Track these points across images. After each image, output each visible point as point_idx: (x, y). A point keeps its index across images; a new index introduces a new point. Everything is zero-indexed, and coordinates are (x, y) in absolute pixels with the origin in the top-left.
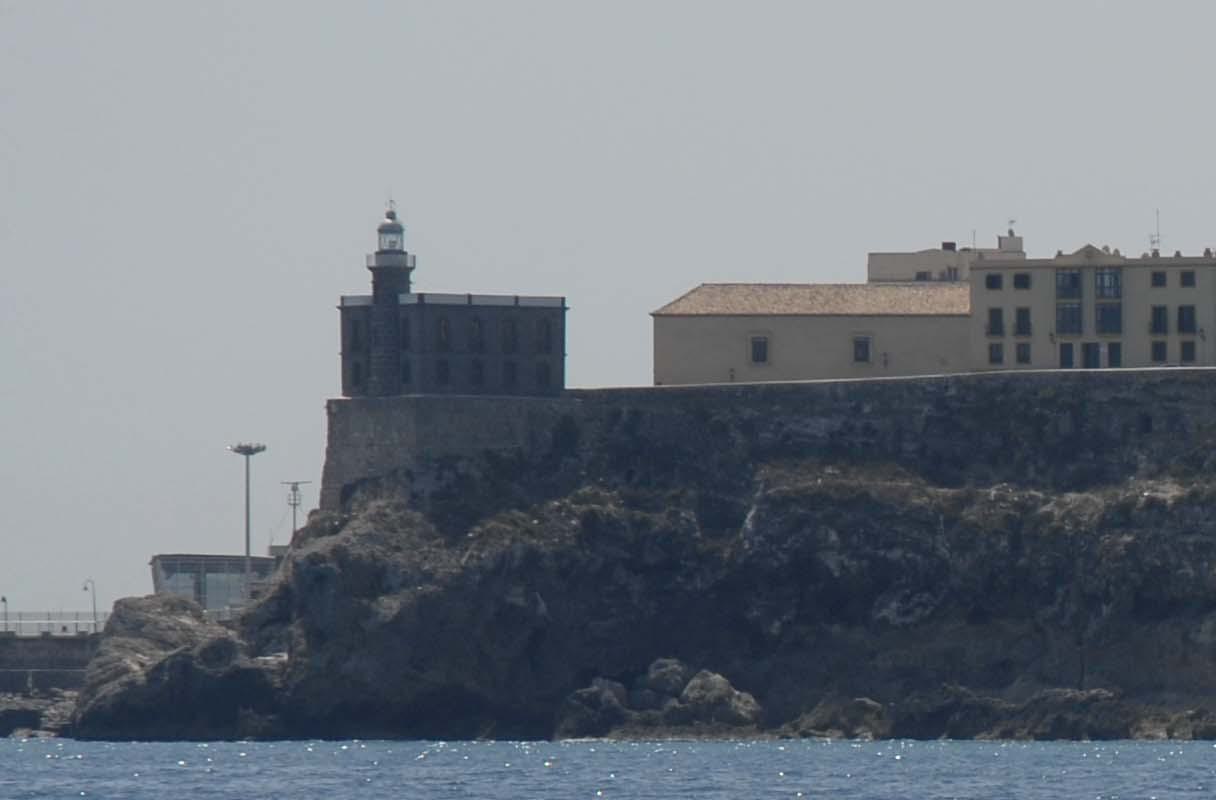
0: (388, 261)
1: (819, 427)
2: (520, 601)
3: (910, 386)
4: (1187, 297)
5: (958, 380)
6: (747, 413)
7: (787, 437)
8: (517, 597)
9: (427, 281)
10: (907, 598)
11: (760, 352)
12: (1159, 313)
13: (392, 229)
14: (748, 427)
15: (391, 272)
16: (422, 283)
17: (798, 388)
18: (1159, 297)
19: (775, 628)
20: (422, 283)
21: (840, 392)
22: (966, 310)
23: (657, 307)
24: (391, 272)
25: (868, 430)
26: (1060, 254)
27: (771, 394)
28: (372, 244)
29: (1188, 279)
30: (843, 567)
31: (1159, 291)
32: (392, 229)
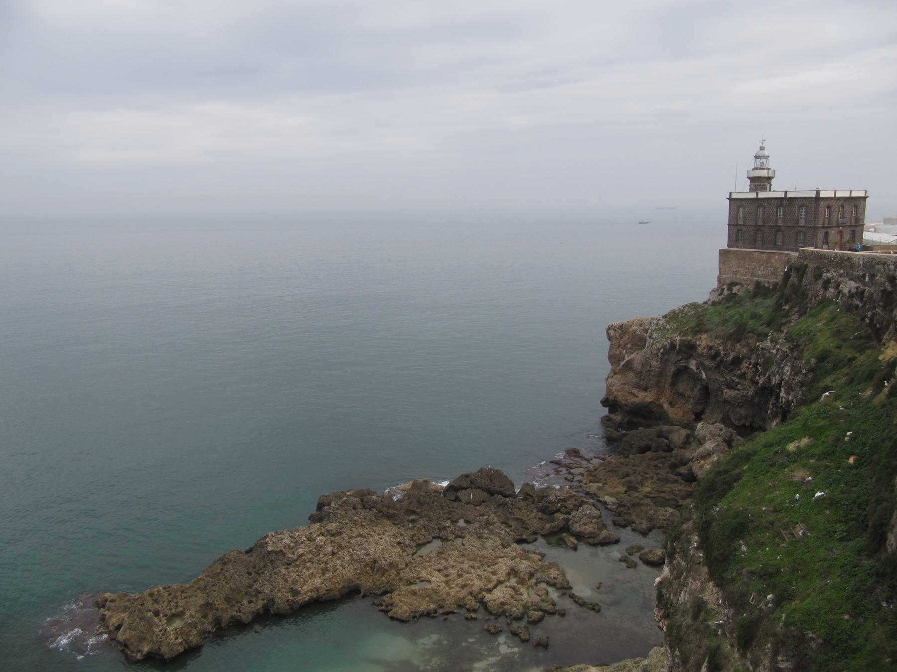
2: (694, 368)
15: (759, 183)
20: (778, 189)
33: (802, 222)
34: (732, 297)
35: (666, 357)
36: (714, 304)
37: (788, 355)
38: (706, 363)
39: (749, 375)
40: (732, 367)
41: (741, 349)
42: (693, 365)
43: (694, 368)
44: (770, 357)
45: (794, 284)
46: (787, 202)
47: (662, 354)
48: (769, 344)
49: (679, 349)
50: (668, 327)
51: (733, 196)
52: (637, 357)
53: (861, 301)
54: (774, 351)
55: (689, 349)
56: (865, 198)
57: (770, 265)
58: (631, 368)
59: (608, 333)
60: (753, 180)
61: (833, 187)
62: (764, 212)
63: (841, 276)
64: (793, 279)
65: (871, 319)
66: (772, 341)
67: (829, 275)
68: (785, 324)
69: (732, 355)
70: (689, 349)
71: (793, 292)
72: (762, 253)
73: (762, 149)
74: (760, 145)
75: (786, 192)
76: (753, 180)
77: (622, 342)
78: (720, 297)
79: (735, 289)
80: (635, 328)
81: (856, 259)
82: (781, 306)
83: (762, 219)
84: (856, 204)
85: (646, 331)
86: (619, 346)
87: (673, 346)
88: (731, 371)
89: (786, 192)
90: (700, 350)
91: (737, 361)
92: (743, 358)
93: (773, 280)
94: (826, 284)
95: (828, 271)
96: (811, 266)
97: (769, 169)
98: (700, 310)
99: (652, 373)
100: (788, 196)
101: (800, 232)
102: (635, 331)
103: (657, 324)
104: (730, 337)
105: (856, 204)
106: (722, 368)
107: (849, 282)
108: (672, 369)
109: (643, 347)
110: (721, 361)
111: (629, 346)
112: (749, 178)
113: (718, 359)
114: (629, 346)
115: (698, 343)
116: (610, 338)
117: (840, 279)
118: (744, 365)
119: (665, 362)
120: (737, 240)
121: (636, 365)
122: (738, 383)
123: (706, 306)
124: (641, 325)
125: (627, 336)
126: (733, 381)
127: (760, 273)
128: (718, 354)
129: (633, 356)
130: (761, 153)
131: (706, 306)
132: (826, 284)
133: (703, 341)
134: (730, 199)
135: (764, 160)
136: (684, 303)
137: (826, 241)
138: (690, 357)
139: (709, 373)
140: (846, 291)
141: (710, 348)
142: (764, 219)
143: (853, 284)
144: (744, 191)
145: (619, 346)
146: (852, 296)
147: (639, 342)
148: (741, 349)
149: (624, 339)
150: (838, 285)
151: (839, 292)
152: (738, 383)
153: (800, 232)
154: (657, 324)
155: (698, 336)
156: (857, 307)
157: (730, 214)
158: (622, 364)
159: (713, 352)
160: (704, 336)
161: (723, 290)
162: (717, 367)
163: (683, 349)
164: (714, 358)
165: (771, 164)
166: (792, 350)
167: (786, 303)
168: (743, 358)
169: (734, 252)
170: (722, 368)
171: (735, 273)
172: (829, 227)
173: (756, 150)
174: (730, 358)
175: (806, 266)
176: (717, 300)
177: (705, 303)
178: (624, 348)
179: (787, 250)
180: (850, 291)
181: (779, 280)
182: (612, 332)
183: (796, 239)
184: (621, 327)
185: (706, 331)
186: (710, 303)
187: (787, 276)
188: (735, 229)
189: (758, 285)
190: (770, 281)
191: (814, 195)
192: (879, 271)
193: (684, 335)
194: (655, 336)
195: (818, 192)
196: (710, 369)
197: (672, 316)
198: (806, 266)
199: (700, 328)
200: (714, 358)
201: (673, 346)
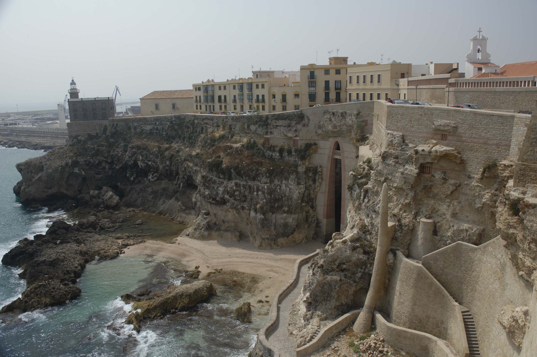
0: (74, 91)
1: (148, 128)
2: (78, 172)
3: (165, 117)
4: (338, 77)
5: (175, 116)
6: (136, 124)
7: (142, 130)
8: (76, 170)
9: (84, 94)
10: (152, 175)
11: (157, 107)
12: (327, 83)
13: (73, 83)
14: (135, 128)
15: (74, 94)
16: (81, 96)
17: (144, 118)
18: (327, 78)
19: (132, 179)
20: (81, 96)
21: (152, 119)
22: (299, 81)
23: (141, 97)
24: (74, 94)
25: (157, 129)
26: (228, 80)
27: (140, 120)
28: (69, 87)
29: (225, 88)
30: (141, 166)
31: (338, 76)
32: (73, 83)
38: (85, 168)
86: (28, 172)
90: (81, 163)
91: (100, 163)
118: (104, 164)
128: (90, 162)
132: (135, 128)
145: (28, 172)
164: (88, 165)
165: (78, 87)
190: (93, 133)
200: (88, 165)
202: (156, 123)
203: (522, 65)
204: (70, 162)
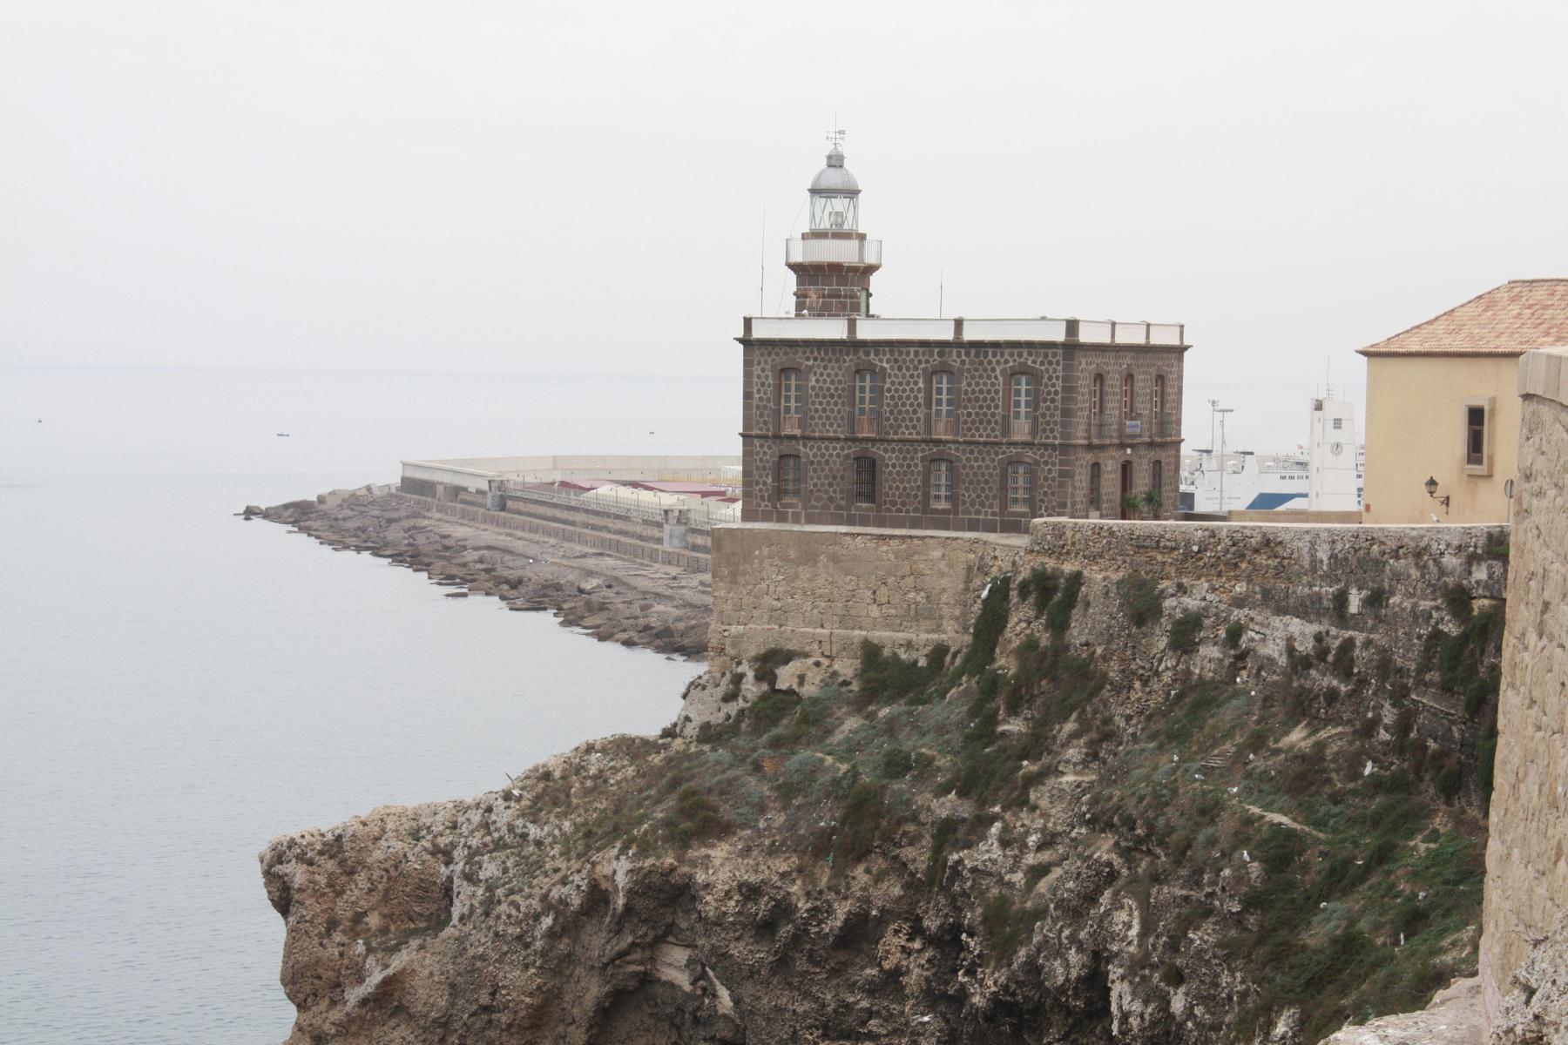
1: (1279, 636)
2: (683, 980)
13: (834, 187)
15: (832, 283)
20: (901, 307)
24: (832, 283)
28: (800, 214)
32: (834, 187)
33: (1021, 430)
34: (777, 704)
35: (563, 946)
36: (709, 734)
37: (1113, 876)
38: (737, 950)
39: (915, 977)
40: (842, 956)
41: (870, 885)
42: (675, 966)
43: (683, 980)
44: (1003, 901)
45: (1030, 645)
46: (955, 358)
47: (551, 934)
48: (997, 853)
49: (628, 908)
50: (534, 831)
51: (758, 333)
52: (422, 963)
53: (1347, 674)
54: (1018, 878)
55: (664, 901)
56: (1179, 351)
57: (913, 583)
58: (400, 1009)
59: (270, 876)
60: (806, 273)
61: (1113, 311)
62: (878, 392)
63: (1239, 602)
64: (1021, 623)
65: (1403, 727)
66: (1005, 843)
67: (1192, 603)
68: (1037, 779)
69: (842, 910)
70: (664, 901)
71: (1024, 677)
72: (882, 537)
73: (835, 161)
74: (828, 148)
75: (959, 323)
76: (806, 273)
77: (343, 910)
78: (732, 709)
79: (786, 677)
80: (398, 846)
81: (1304, 546)
82: (992, 720)
83: (851, 410)
84: (1156, 365)
85: (446, 855)
86: (332, 925)
87: (597, 897)
88: (835, 972)
89: (959, 323)
90: (709, 904)
91: (859, 933)
92: (885, 917)
93: (924, 637)
94: (1186, 634)
95: (1182, 589)
96: (1098, 578)
97: (862, 237)
98: (656, 759)
99: (504, 1018)
100: (969, 335)
101: (1014, 462)
102: (399, 861)
103: (486, 826)
104: (820, 846)
105: (1156, 365)
106: (801, 964)
107: (1277, 621)
108: (593, 990)
109: (439, 921)
110: (796, 939)
111: (373, 920)
112: (794, 267)
113: (786, 930)
114: (373, 920)
115: (700, 877)
116: (283, 901)
117: (1238, 614)
118: (892, 942)
119: (559, 966)
120: (779, 493)
121: (427, 995)
122: (871, 1014)
123: (678, 744)
124: (415, 835)
125: (361, 878)
126: (848, 1007)
127: (875, 611)
128: (783, 909)
129: (398, 962)
130: (833, 179)
131: (678, 744)
132: (1186, 634)
133: (720, 867)
134: (747, 342)
135: (839, 204)
136: (580, 740)
137: (1094, 501)
138: (667, 934)
139: (748, 990)
140: (1273, 649)
141: (751, 892)
142: (878, 417)
143: (1302, 631)
144: (781, 317)
145: (332, 925)
146: (1299, 663)
147: (420, 903)
148: (870, 885)
149: (353, 893)
150: (1235, 633)
151: (1242, 657)
152: (871, 1014)
153: (1014, 462)
154: (486, 826)
155: (695, 853)
156: (1332, 696)
157: (747, 395)
158: (354, 995)
159: (763, 906)
160: (720, 852)
161: (738, 679)
162: (783, 962)
163: (641, 904)
164: (765, 929)
165: (867, 216)
166: (1127, 854)
167: (1013, 710)
168: (882, 921)
169: (767, 537)
170: (801, 964)
171: (779, 615)
172: (1102, 447)
173: (813, 167)
174: (836, 922)
175: (1077, 579)
176: (718, 718)
177: (669, 733)
178: (353, 933)
179: (973, 526)
180: (1290, 650)
181: (955, 636)
182: (297, 874)
183: (1004, 487)
184: (334, 846)
185: (724, 830)
186: (691, 730)
187: (991, 623)
188: (770, 452)
189: (871, 653)
190: (910, 641)
191: (1059, 336)
192: (1397, 577)
193: (644, 852)
194: (489, 869)
195: (1072, 326)
196: (752, 973)
197: (546, 791)
198: (1077, 579)
199: (700, 821)
200: (765, 929)
201: (597, 897)
202: (1341, 599)
203: (1368, 399)
204: (622, 880)
